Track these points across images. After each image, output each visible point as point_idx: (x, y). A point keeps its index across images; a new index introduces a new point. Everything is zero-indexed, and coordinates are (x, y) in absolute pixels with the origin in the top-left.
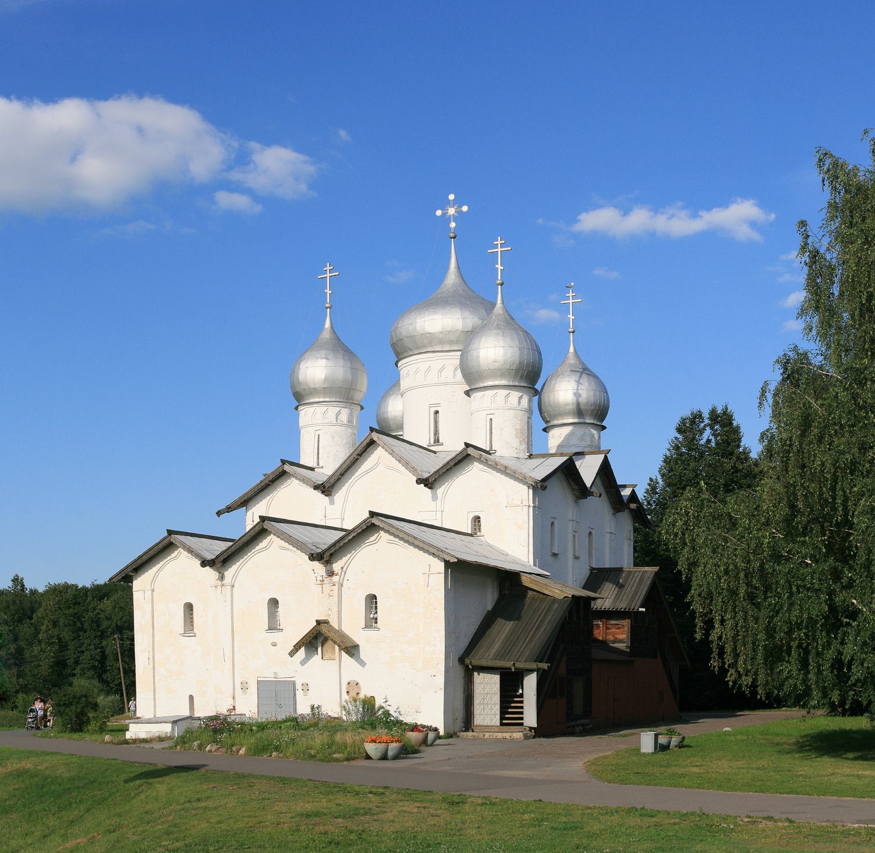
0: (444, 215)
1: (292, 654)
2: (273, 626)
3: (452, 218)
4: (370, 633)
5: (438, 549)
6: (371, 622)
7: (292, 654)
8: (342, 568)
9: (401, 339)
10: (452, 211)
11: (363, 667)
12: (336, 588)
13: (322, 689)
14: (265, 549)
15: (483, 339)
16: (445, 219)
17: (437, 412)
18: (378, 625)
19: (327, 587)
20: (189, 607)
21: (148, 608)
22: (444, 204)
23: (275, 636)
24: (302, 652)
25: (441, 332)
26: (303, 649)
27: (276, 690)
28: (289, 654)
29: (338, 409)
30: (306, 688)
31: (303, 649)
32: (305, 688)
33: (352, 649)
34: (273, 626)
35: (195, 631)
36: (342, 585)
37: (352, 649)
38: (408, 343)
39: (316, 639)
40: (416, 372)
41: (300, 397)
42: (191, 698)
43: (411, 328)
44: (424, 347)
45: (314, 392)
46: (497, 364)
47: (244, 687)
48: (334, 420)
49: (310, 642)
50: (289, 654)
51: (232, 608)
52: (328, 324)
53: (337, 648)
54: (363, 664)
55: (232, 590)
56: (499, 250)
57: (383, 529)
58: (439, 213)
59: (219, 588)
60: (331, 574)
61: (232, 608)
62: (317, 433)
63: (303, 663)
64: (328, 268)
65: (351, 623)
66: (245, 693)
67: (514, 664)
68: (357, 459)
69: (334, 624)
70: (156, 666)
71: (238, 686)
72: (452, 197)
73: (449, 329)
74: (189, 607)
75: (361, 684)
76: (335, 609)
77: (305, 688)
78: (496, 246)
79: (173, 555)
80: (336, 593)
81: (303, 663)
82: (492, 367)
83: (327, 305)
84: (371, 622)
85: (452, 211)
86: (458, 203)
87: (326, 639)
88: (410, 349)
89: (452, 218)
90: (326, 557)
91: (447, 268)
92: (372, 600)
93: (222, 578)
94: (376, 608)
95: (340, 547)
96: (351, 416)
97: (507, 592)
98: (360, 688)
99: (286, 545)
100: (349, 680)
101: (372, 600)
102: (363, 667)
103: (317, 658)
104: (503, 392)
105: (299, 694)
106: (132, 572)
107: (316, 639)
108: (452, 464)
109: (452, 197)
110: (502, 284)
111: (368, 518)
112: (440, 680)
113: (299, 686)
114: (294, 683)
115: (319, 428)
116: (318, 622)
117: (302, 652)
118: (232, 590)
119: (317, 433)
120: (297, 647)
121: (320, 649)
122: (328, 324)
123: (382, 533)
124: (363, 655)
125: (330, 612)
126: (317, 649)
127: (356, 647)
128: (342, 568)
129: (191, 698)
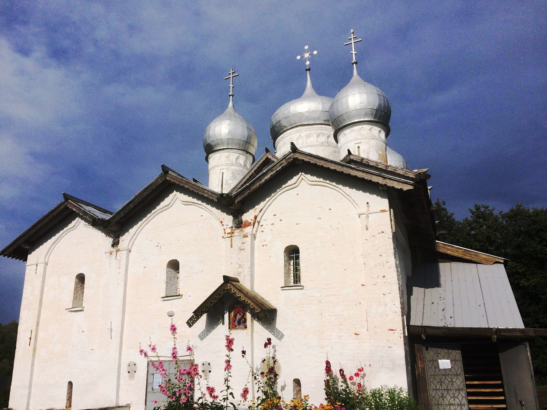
1: (191, 322)
2: (172, 294)
3: (307, 59)
4: (294, 293)
7: (191, 322)
12: (248, 240)
26: (204, 317)
28: (188, 323)
29: (237, 155)
31: (204, 317)
35: (84, 305)
37: (267, 315)
38: (284, 123)
41: (210, 149)
43: (286, 112)
48: (234, 163)
51: (126, 275)
60: (239, 225)
63: (202, 336)
65: (265, 282)
66: (132, 377)
70: (38, 347)
73: (314, 110)
74: (81, 278)
79: (70, 226)
80: (248, 246)
81: (202, 336)
82: (358, 108)
83: (231, 94)
88: (285, 127)
89: (307, 59)
91: (306, 80)
92: (293, 253)
93: (115, 244)
96: (246, 161)
99: (190, 199)
101: (293, 253)
104: (367, 127)
108: (255, 301)
109: (306, 47)
110: (356, 63)
115: (221, 168)
116: (227, 279)
118: (128, 257)
119: (222, 171)
120: (198, 314)
124: (280, 322)
125: (240, 270)
127: (273, 312)
129: (70, 384)
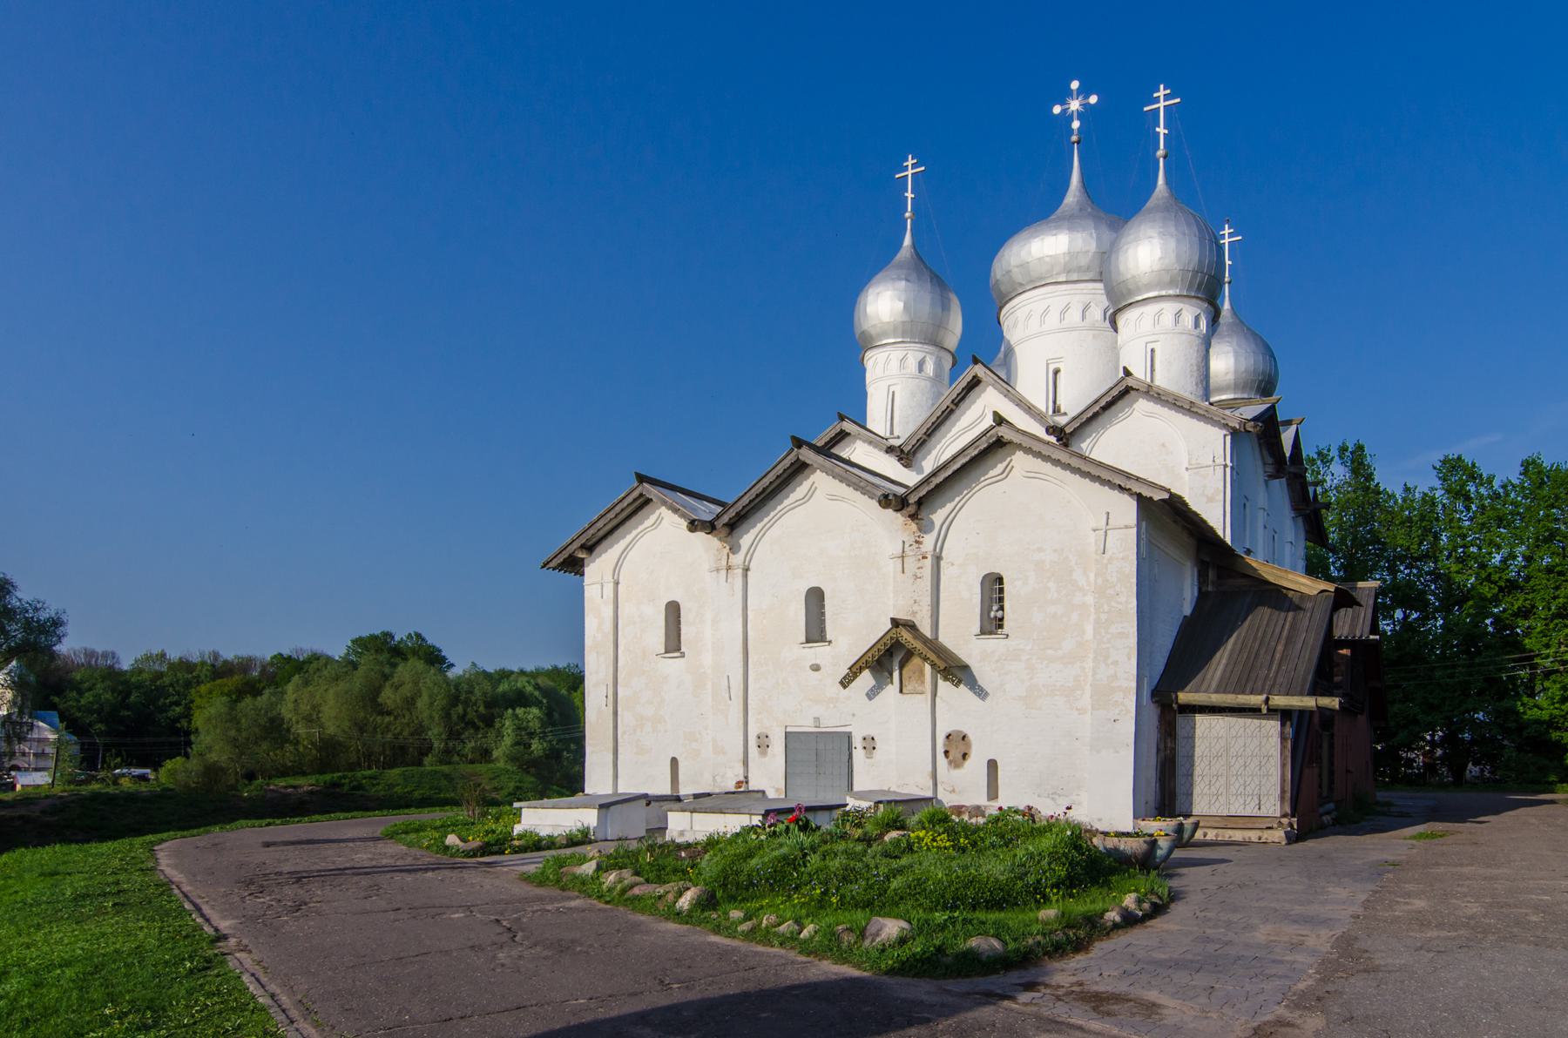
0: (1064, 111)
1: (845, 683)
2: (816, 632)
4: (992, 643)
5: (1128, 476)
6: (993, 624)
7: (845, 683)
10: (1075, 105)
11: (983, 699)
12: (928, 562)
13: (897, 751)
16: (1066, 118)
17: (1056, 372)
18: (1006, 630)
21: (608, 611)
22: (1064, 96)
23: (818, 652)
24: (866, 679)
26: (866, 674)
27: (820, 750)
30: (870, 744)
32: (869, 745)
33: (955, 671)
34: (816, 632)
37: (955, 671)
39: (894, 655)
40: (1029, 316)
42: (674, 761)
44: (1041, 278)
47: (763, 743)
49: (879, 662)
52: (907, 241)
53: (928, 668)
54: (981, 693)
55: (745, 576)
56: (1162, 105)
57: (1020, 447)
58: (1093, 99)
63: (871, 694)
65: (957, 629)
67: (1267, 699)
68: (952, 411)
72: (1075, 85)
75: (971, 736)
77: (869, 745)
78: (1157, 100)
79: (648, 523)
81: (871, 694)
84: (993, 624)
86: (1084, 92)
87: (910, 654)
90: (912, 505)
94: (1001, 600)
95: (938, 486)
97: (1210, 588)
98: (969, 745)
100: (949, 730)
102: (983, 699)
103: (892, 690)
105: (859, 755)
106: (583, 547)
107: (894, 655)
111: (993, 427)
112: (1127, 728)
113: (857, 742)
114: (849, 736)
116: (896, 623)
117: (866, 679)
118: (745, 576)
121: (896, 674)
122: (907, 241)
123: (1019, 454)
125: (916, 608)
126: (891, 674)
129: (674, 761)
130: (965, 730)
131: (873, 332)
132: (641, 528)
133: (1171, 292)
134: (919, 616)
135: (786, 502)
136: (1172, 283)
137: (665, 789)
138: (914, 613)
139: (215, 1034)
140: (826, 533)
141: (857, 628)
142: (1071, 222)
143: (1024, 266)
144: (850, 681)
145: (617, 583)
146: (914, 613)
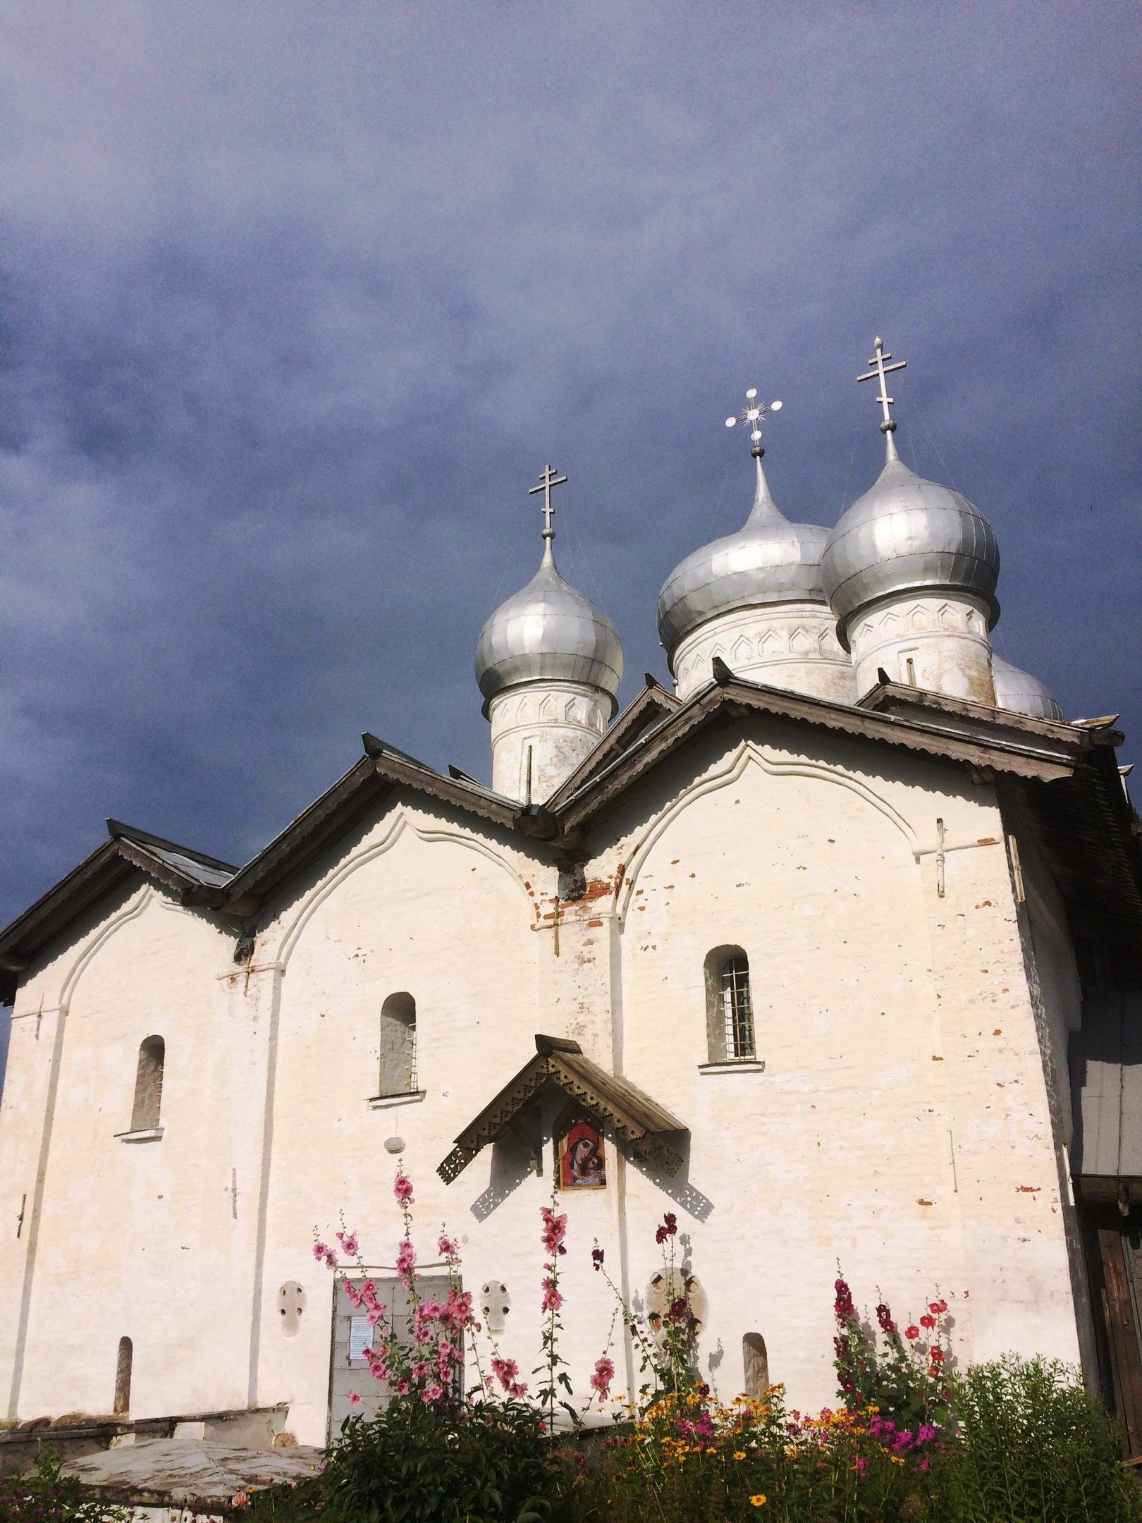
2: (397, 1089)
3: (755, 425)
4: (736, 1083)
6: (736, 1037)
7: (449, 1170)
8: (622, 869)
9: (682, 599)
10: (753, 415)
12: (603, 933)
14: (381, 848)
15: (876, 504)
19: (572, 934)
20: (154, 1049)
25: (760, 569)
26: (486, 1154)
29: (569, 697)
34: (397, 1089)
36: (622, 926)
38: (696, 603)
41: (493, 685)
42: (126, 1344)
43: (701, 573)
45: (523, 663)
46: (916, 543)
50: (474, 1209)
59: (241, 979)
60: (577, 891)
61: (273, 1038)
62: (528, 743)
63: (482, 1209)
64: (547, 473)
65: (654, 1051)
69: (598, 1056)
71: (611, 1257)
73: (778, 562)
74: (154, 1049)
76: (602, 1003)
79: (126, 907)
80: (602, 951)
81: (482, 1209)
83: (546, 531)
84: (736, 1037)
85: (753, 415)
88: (701, 613)
89: (755, 425)
92: (729, 967)
99: (442, 824)
100: (282, 1281)
101: (729, 967)
104: (932, 604)
109: (752, 393)
116: (545, 1045)
118: (277, 989)
119: (528, 743)
120: (468, 1144)
124: (699, 1171)
125: (582, 1018)
128: (622, 869)
129: (126, 1344)
130: (304, 1284)
131: (501, 669)
132: (114, 916)
133: (928, 583)
134: (588, 1032)
135: (355, 851)
136: (928, 570)
137: (100, 1405)
138: (580, 1028)
139: (4, 1502)
140: (422, 906)
141: (471, 1069)
142: (763, 530)
143: (703, 588)
144: (456, 1171)
145: (65, 1012)
146: (580, 1028)
